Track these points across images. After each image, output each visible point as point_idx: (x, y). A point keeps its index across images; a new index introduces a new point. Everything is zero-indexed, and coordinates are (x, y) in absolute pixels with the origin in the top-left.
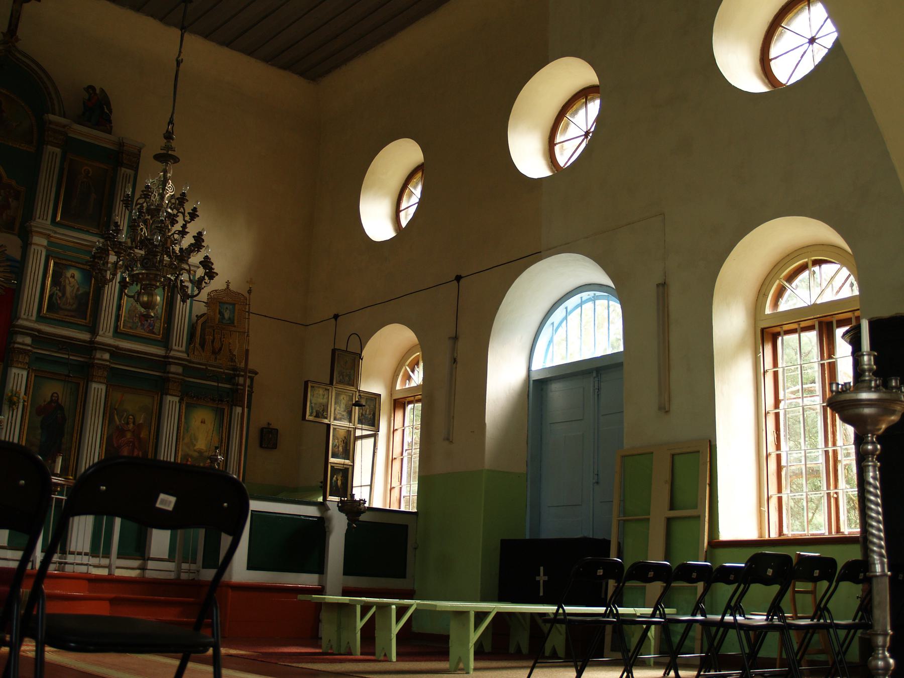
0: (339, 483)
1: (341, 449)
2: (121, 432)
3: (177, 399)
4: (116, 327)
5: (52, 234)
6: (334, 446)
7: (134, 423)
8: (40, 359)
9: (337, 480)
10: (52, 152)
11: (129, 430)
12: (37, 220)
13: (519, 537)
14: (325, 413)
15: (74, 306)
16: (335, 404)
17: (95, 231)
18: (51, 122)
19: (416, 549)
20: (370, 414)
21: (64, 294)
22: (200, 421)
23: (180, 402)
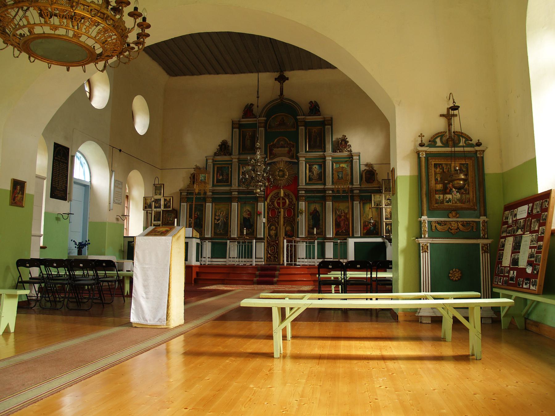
0: (389, 228)
2: (340, 216)
3: (358, 202)
5: (306, 156)
6: (386, 215)
7: (344, 213)
8: (308, 197)
10: (302, 129)
14: (380, 204)
15: (317, 178)
18: (299, 119)
21: (313, 174)
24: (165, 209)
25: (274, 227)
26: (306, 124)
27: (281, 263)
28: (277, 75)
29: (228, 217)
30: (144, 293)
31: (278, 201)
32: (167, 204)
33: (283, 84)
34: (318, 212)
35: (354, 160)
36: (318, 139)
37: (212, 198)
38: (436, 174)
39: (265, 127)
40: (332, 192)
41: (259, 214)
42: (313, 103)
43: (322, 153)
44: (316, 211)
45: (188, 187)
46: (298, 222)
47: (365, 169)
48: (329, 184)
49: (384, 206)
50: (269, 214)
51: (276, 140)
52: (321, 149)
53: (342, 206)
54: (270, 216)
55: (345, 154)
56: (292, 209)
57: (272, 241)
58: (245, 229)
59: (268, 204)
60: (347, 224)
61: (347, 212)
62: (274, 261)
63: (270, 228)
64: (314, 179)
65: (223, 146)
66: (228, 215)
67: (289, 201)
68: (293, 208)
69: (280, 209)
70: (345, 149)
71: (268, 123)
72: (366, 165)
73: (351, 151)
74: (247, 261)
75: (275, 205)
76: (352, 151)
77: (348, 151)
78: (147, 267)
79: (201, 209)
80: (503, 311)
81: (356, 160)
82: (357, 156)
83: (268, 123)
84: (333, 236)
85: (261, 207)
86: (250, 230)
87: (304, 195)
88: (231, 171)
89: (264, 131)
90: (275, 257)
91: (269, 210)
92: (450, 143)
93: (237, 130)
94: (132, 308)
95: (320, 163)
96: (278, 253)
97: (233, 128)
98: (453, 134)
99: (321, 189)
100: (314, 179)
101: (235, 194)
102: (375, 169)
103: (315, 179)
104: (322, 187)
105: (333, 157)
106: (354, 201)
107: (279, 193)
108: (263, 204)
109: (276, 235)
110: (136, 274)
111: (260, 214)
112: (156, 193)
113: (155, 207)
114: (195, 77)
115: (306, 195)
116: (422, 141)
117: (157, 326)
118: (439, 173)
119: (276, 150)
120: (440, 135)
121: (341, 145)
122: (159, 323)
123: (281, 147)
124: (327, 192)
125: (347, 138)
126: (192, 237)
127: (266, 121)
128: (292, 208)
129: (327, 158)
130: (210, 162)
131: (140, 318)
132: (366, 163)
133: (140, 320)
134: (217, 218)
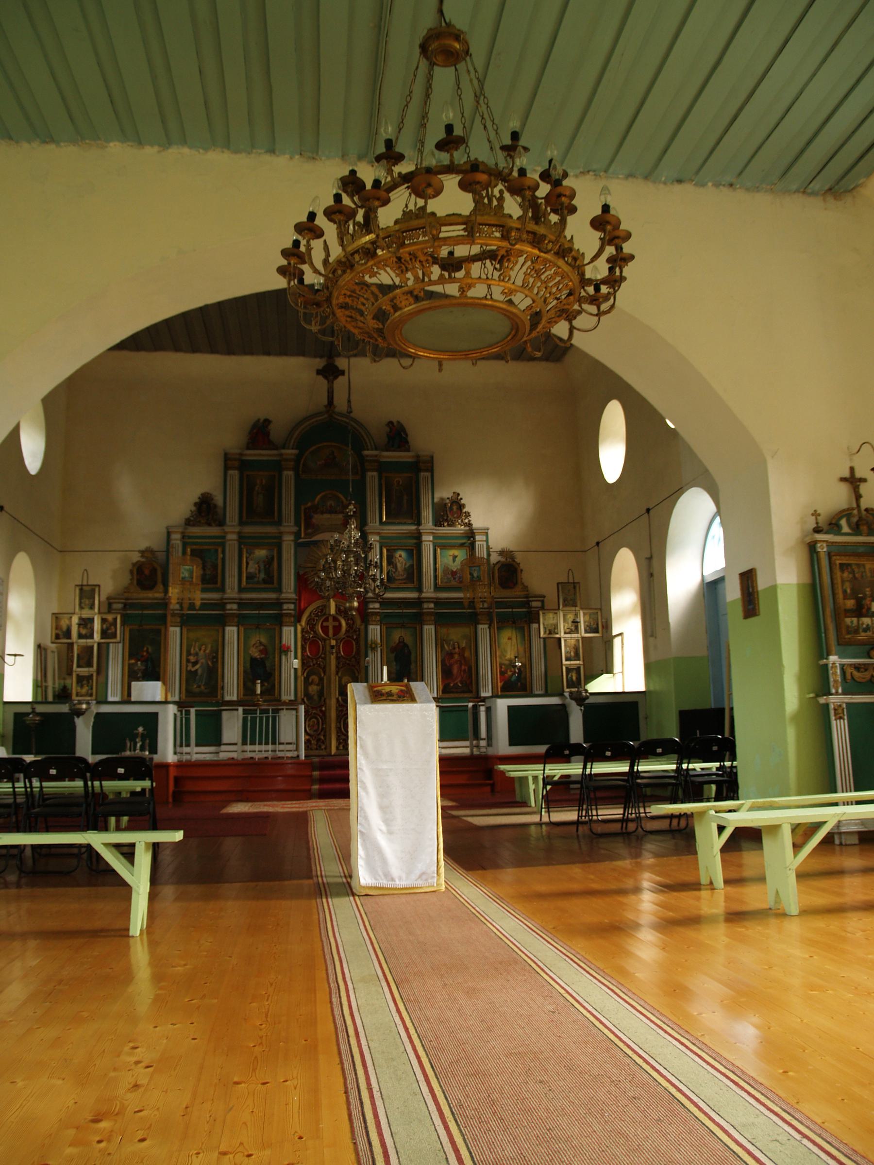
0: (574, 678)
1: (572, 654)
2: (451, 655)
3: (487, 626)
4: (436, 584)
5: (381, 532)
6: (566, 653)
7: (459, 648)
8: (387, 615)
9: (572, 676)
10: (372, 477)
11: (456, 653)
12: (370, 524)
13: (708, 707)
14: (556, 631)
15: (405, 576)
16: (564, 622)
17: (410, 521)
18: (367, 456)
19: (646, 718)
20: (594, 624)
21: (396, 569)
22: (507, 638)
23: (489, 628)
24: (103, 641)
25: (315, 678)
26: (382, 468)
27: (333, 753)
28: (319, 363)
29: (216, 657)
30: (382, 823)
31: (325, 624)
32: (108, 629)
33: (333, 383)
34: (407, 646)
35: (477, 543)
36: (405, 498)
37: (239, 616)
38: (843, 581)
39: (296, 469)
40: (435, 606)
41: (285, 651)
42: (395, 424)
43: (413, 527)
44: (402, 645)
45: (125, 592)
46: (367, 667)
47: (499, 561)
48: (429, 591)
49: (562, 634)
50: (306, 651)
51: (318, 497)
52: (412, 518)
53: (457, 634)
54: (308, 656)
55: (460, 529)
56: (354, 640)
57: (312, 708)
58: (259, 681)
59: (303, 630)
60: (465, 670)
61: (464, 645)
62: (317, 749)
63: (308, 679)
64: (397, 580)
65: (204, 506)
66: (217, 653)
67: (347, 624)
68: (355, 637)
69: (330, 639)
70: (460, 521)
71: (302, 461)
72: (502, 553)
73: (469, 525)
74: (287, 751)
75: (319, 632)
76: (472, 525)
77: (466, 525)
78: (387, 769)
79: (157, 640)
80: (817, 826)
81: (482, 543)
82: (484, 535)
83: (302, 461)
84: (437, 695)
85: (289, 635)
86: (266, 684)
87: (379, 612)
88: (223, 559)
89: (293, 477)
90: (319, 740)
91: (306, 643)
92: (864, 528)
93: (234, 474)
94: (359, 857)
95: (410, 548)
96: (325, 732)
97: (226, 468)
98: (864, 513)
99: (412, 599)
100: (397, 580)
101: (232, 607)
102: (518, 560)
103: (399, 580)
104: (414, 595)
105: (437, 535)
106: (478, 624)
107: (324, 608)
108: (292, 629)
109: (321, 693)
110: (364, 784)
111: (285, 650)
112: (83, 605)
113: (80, 636)
114: (143, 354)
115: (383, 613)
116: (817, 523)
117: (417, 888)
118: (848, 581)
119: (318, 519)
120: (846, 513)
121: (450, 512)
122: (420, 883)
123: (330, 512)
124: (425, 606)
125: (461, 499)
126: (166, 702)
127: (298, 458)
128: (353, 639)
129: (424, 538)
130: (177, 540)
131: (379, 876)
132: (500, 549)
133: (378, 880)
134: (192, 659)
